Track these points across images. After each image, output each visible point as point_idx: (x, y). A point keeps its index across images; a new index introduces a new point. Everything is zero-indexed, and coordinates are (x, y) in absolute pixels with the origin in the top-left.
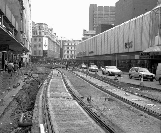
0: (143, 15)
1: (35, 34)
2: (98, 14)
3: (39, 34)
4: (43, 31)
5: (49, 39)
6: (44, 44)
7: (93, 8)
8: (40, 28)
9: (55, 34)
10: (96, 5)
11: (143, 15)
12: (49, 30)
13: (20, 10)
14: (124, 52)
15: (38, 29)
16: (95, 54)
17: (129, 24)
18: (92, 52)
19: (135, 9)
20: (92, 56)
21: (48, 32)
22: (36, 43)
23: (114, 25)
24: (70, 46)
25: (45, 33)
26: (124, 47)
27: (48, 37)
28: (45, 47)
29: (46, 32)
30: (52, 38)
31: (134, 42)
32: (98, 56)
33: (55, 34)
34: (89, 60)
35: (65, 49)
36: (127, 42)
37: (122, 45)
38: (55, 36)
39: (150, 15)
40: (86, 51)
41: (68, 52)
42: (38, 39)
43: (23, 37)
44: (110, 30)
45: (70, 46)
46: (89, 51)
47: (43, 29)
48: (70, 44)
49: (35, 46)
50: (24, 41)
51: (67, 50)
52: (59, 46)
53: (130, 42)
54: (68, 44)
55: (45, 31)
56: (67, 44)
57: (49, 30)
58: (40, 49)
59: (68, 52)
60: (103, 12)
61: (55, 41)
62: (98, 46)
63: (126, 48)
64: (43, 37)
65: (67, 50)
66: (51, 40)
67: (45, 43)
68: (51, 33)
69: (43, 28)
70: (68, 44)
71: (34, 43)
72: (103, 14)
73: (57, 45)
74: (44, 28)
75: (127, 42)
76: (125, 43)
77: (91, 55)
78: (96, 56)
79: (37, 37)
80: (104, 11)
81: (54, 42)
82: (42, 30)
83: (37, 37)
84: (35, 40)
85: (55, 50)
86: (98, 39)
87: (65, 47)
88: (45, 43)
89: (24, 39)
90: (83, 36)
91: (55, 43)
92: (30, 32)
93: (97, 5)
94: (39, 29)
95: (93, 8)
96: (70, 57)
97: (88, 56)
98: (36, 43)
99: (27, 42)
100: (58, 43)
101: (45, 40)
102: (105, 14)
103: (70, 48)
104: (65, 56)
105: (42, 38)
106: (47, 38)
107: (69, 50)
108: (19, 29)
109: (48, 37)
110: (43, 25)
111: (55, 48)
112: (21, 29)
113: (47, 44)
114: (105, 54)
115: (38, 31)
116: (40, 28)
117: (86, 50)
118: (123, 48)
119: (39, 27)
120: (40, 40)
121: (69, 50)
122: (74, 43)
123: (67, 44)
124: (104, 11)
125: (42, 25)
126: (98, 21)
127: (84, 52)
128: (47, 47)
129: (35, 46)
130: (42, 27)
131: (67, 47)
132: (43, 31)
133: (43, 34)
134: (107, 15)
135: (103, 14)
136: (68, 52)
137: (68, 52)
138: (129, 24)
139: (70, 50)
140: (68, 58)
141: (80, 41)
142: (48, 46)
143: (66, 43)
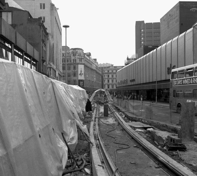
0: (186, 33)
1: (69, 61)
2: (147, 33)
3: (74, 61)
4: (78, 57)
5: (86, 66)
6: (79, 73)
7: (140, 25)
8: (74, 54)
9: (95, 60)
10: (143, 21)
11: (185, 32)
12: (86, 56)
13: (40, 36)
14: (167, 79)
15: (72, 55)
16: (136, 82)
17: (171, 44)
18: (134, 80)
19: (182, 24)
20: (134, 85)
21: (83, 59)
22: (70, 71)
23: (151, 47)
24: (111, 73)
25: (81, 59)
26: (167, 72)
27: (84, 64)
28: (81, 76)
29: (82, 58)
30: (89, 65)
31: (177, 66)
32: (140, 84)
33: (95, 60)
34: (131, 90)
35: (105, 77)
36: (169, 67)
37: (164, 70)
38: (94, 63)
39: (192, 32)
40: (127, 79)
41: (108, 81)
42: (72, 66)
43: (49, 66)
44: (151, 52)
45: (111, 73)
46: (131, 79)
47: (78, 55)
48: (110, 71)
49: (69, 76)
50: (50, 70)
51: (107, 79)
52: (99, 74)
53: (172, 66)
54: (108, 71)
55: (80, 57)
56: (106, 71)
57: (86, 56)
58: (75, 78)
59: (108, 81)
60: (153, 30)
61: (94, 68)
62: (137, 73)
63: (169, 74)
64: (78, 64)
65: (107, 79)
66: (88, 67)
67: (81, 71)
68: (89, 59)
69: (78, 53)
70: (108, 71)
71: (68, 71)
72: (153, 32)
73: (97, 72)
74: (79, 54)
75: (169, 67)
76: (168, 68)
77: (133, 83)
78: (138, 84)
79: (71, 64)
80: (154, 28)
81: (92, 69)
82: (77, 57)
83: (71, 64)
84: (69, 69)
85: (95, 79)
86: (139, 64)
87: (105, 75)
88: (81, 71)
89: (50, 68)
90: (126, 61)
91: (94, 70)
92: (61, 60)
93: (145, 22)
94: (74, 55)
95: (140, 25)
96: (110, 87)
97: (129, 85)
98: (70, 71)
99: (55, 71)
100: (98, 71)
101: (81, 68)
102: (155, 33)
103: (110, 76)
104: (105, 86)
105: (77, 66)
106: (83, 65)
107: (109, 79)
108: (40, 58)
109: (84, 64)
110: (79, 50)
111: (95, 76)
112: (43, 58)
113: (83, 72)
114: (154, 81)
115: (73, 58)
116: (74, 54)
117: (127, 78)
118: (166, 73)
119: (73, 53)
120: (75, 68)
121: (109, 79)
122: (115, 70)
123: (106, 71)
124: (146, 29)
125: (77, 50)
126: (147, 41)
127: (125, 80)
128: (83, 76)
129: (69, 76)
130: (77, 53)
131: (107, 75)
132: (78, 57)
133: (78, 61)
134: (158, 33)
135: (153, 32)
136: (108, 81)
137: (108, 81)
138: (171, 44)
139: (111, 79)
140: (108, 87)
141: (123, 67)
142: (85, 75)
143: (110, 70)
